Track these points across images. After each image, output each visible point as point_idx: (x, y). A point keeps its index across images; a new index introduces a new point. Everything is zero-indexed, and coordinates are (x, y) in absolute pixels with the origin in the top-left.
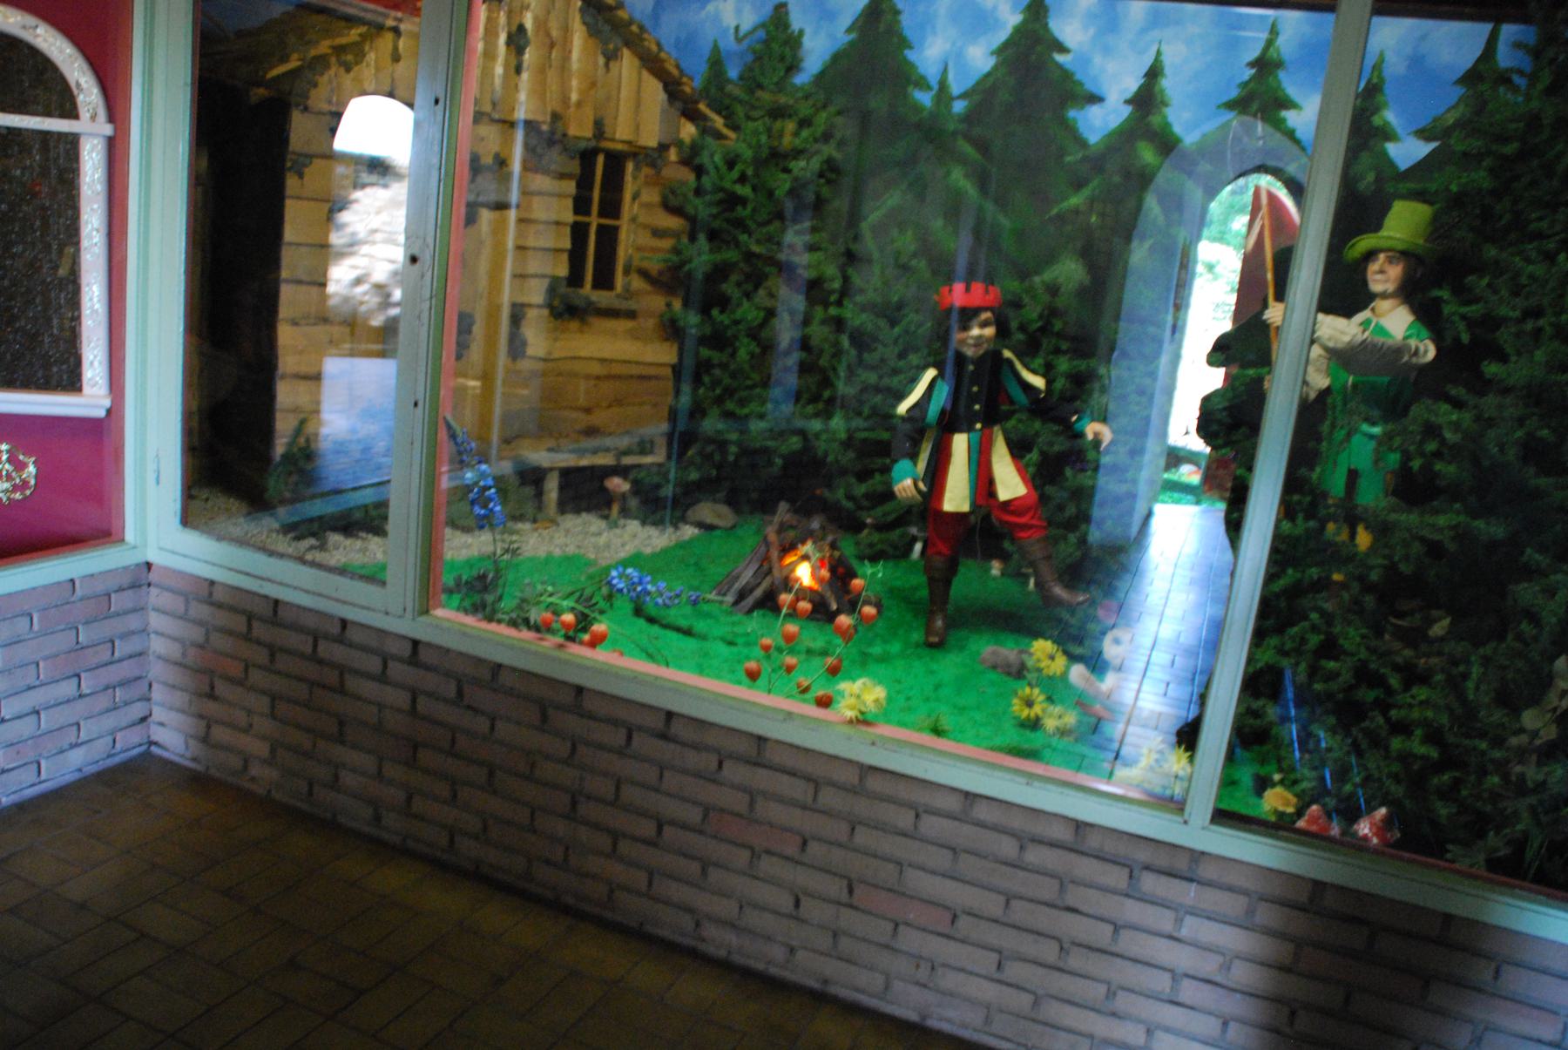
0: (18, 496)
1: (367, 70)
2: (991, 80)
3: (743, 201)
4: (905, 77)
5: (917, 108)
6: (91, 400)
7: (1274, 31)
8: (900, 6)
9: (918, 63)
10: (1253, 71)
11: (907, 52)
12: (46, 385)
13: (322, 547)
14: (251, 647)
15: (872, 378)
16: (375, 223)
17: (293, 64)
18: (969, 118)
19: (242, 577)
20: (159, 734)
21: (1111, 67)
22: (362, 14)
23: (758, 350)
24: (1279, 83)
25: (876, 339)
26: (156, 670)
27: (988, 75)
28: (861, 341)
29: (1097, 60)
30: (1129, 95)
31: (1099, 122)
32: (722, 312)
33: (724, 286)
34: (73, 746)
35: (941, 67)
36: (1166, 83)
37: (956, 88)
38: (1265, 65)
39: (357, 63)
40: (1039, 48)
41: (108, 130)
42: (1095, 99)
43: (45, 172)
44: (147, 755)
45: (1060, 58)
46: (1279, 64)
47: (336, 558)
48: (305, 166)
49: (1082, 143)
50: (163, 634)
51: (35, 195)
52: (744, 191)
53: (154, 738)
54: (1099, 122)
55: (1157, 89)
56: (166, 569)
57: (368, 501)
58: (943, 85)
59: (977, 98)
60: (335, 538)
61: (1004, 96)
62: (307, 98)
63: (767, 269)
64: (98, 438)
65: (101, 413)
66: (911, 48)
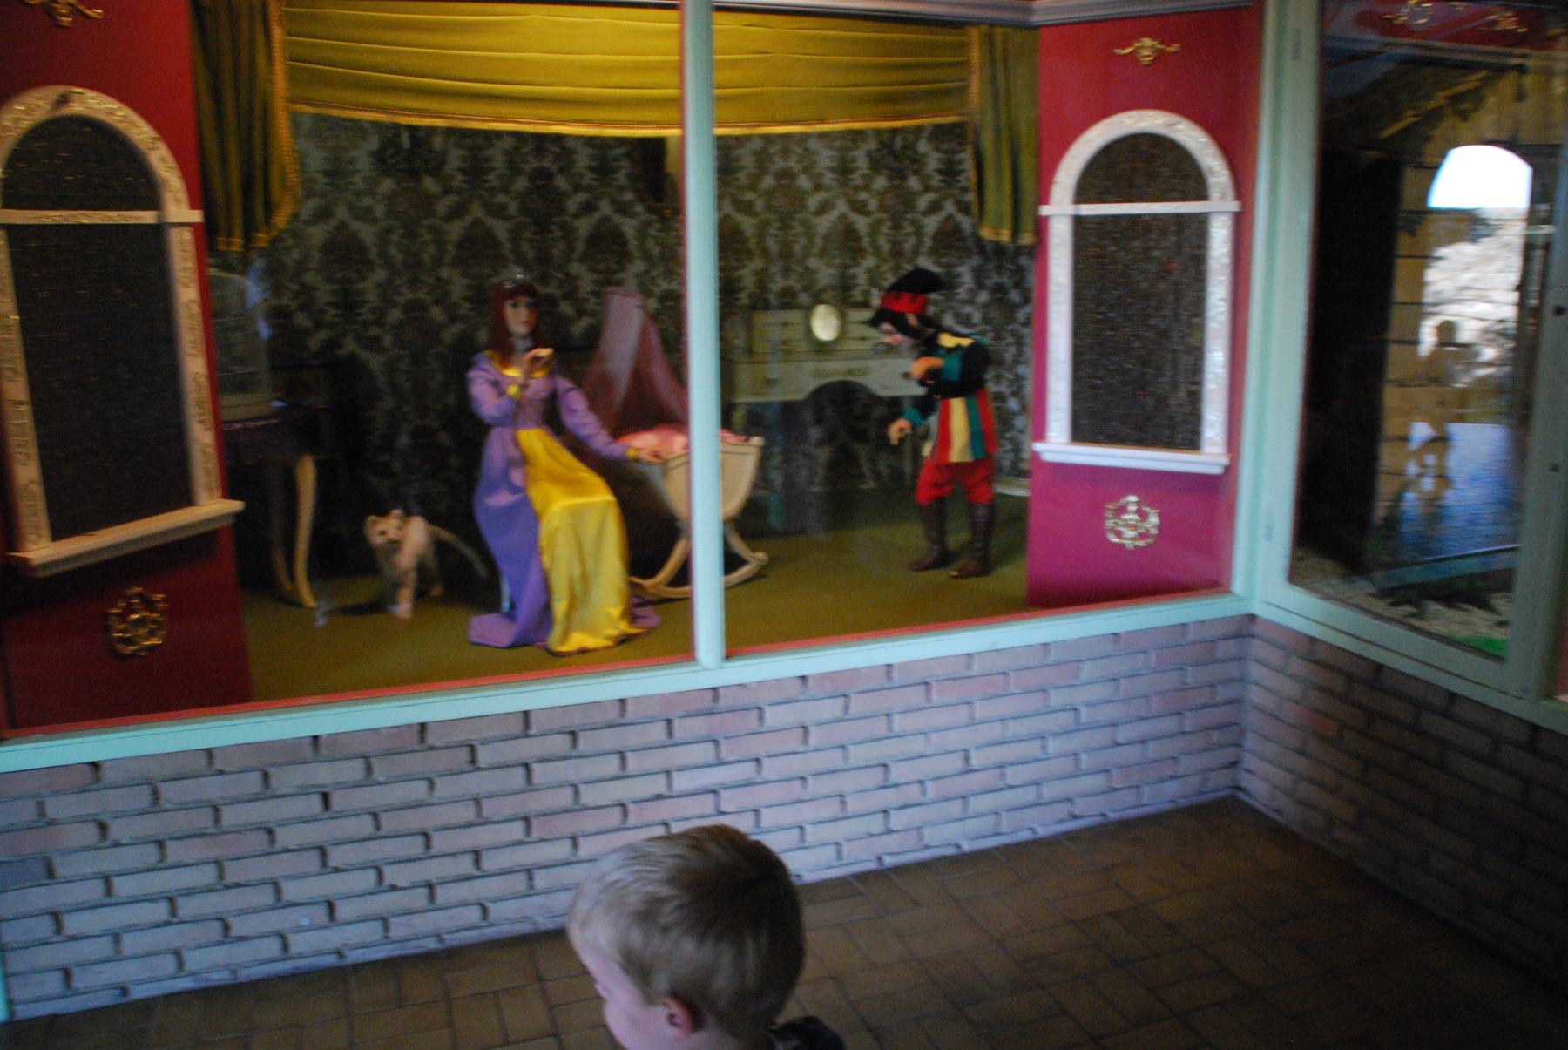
0: (1141, 543)
1: (1486, 119)
6: (1209, 457)
12: (1170, 444)
13: (1420, 615)
14: (1357, 705)
16: (1466, 278)
17: (1409, 120)
19: (1346, 638)
20: (1247, 781)
22: (1480, 59)
26: (1252, 719)
34: (1172, 778)
39: (1475, 109)
41: (1234, 206)
43: (1179, 249)
44: (1233, 798)
47: (1437, 627)
48: (1418, 223)
50: (1270, 686)
51: (1170, 272)
53: (1243, 784)
56: (1266, 621)
57: (1477, 570)
60: (1434, 607)
62: (1420, 155)
64: (1210, 497)
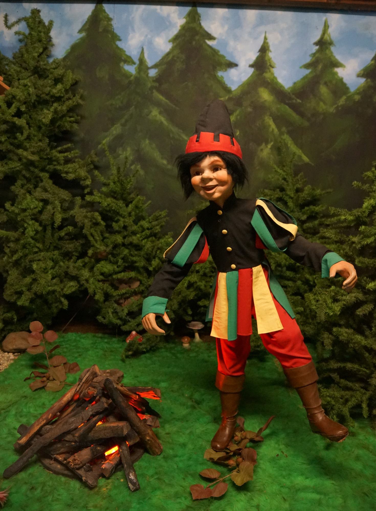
2: (171, 56)
3: (20, 129)
4: (118, 57)
5: (127, 75)
7: (326, 26)
8: (111, 16)
9: (125, 49)
10: (317, 47)
11: (118, 43)
15: (119, 239)
18: (159, 80)
21: (240, 47)
23: (40, 229)
24: (332, 53)
25: (118, 214)
27: (168, 54)
28: (108, 217)
29: (232, 43)
30: (251, 62)
31: (237, 77)
32: (12, 205)
33: (13, 188)
35: (140, 50)
36: (272, 55)
37: (150, 62)
38: (323, 44)
40: (197, 38)
42: (232, 65)
45: (210, 43)
46: (331, 43)
49: (228, 90)
52: (20, 122)
54: (237, 77)
55: (267, 58)
58: (142, 61)
59: (164, 67)
61: (179, 66)
63: (42, 174)
65: (154, 315)
66: (120, 40)
